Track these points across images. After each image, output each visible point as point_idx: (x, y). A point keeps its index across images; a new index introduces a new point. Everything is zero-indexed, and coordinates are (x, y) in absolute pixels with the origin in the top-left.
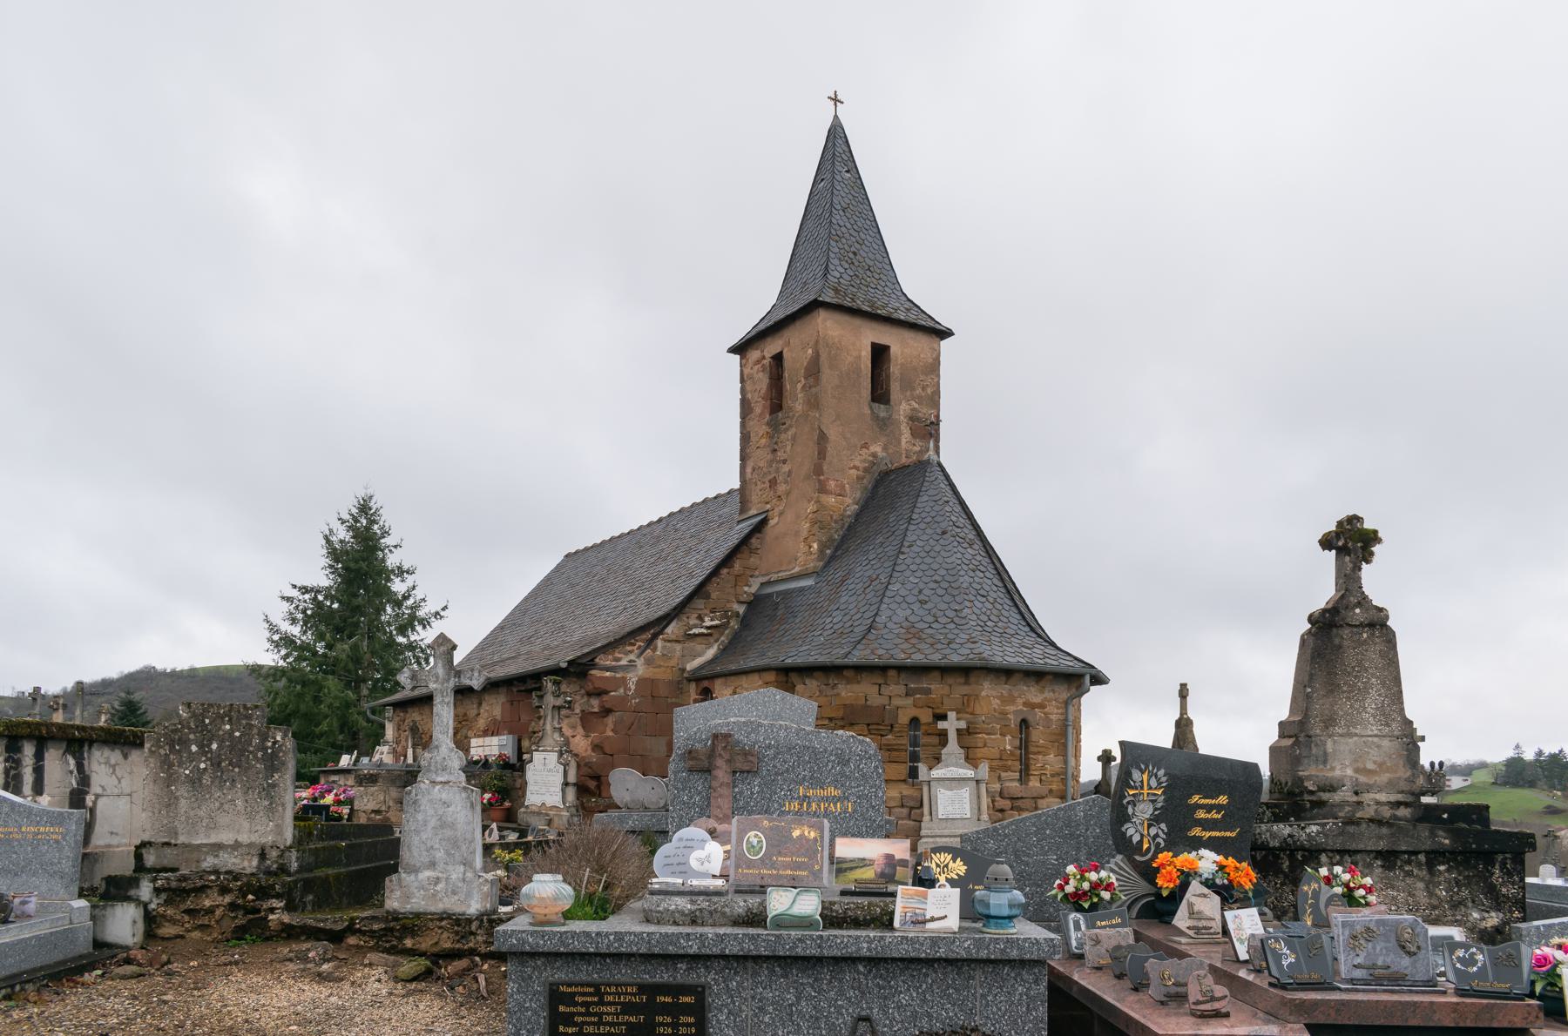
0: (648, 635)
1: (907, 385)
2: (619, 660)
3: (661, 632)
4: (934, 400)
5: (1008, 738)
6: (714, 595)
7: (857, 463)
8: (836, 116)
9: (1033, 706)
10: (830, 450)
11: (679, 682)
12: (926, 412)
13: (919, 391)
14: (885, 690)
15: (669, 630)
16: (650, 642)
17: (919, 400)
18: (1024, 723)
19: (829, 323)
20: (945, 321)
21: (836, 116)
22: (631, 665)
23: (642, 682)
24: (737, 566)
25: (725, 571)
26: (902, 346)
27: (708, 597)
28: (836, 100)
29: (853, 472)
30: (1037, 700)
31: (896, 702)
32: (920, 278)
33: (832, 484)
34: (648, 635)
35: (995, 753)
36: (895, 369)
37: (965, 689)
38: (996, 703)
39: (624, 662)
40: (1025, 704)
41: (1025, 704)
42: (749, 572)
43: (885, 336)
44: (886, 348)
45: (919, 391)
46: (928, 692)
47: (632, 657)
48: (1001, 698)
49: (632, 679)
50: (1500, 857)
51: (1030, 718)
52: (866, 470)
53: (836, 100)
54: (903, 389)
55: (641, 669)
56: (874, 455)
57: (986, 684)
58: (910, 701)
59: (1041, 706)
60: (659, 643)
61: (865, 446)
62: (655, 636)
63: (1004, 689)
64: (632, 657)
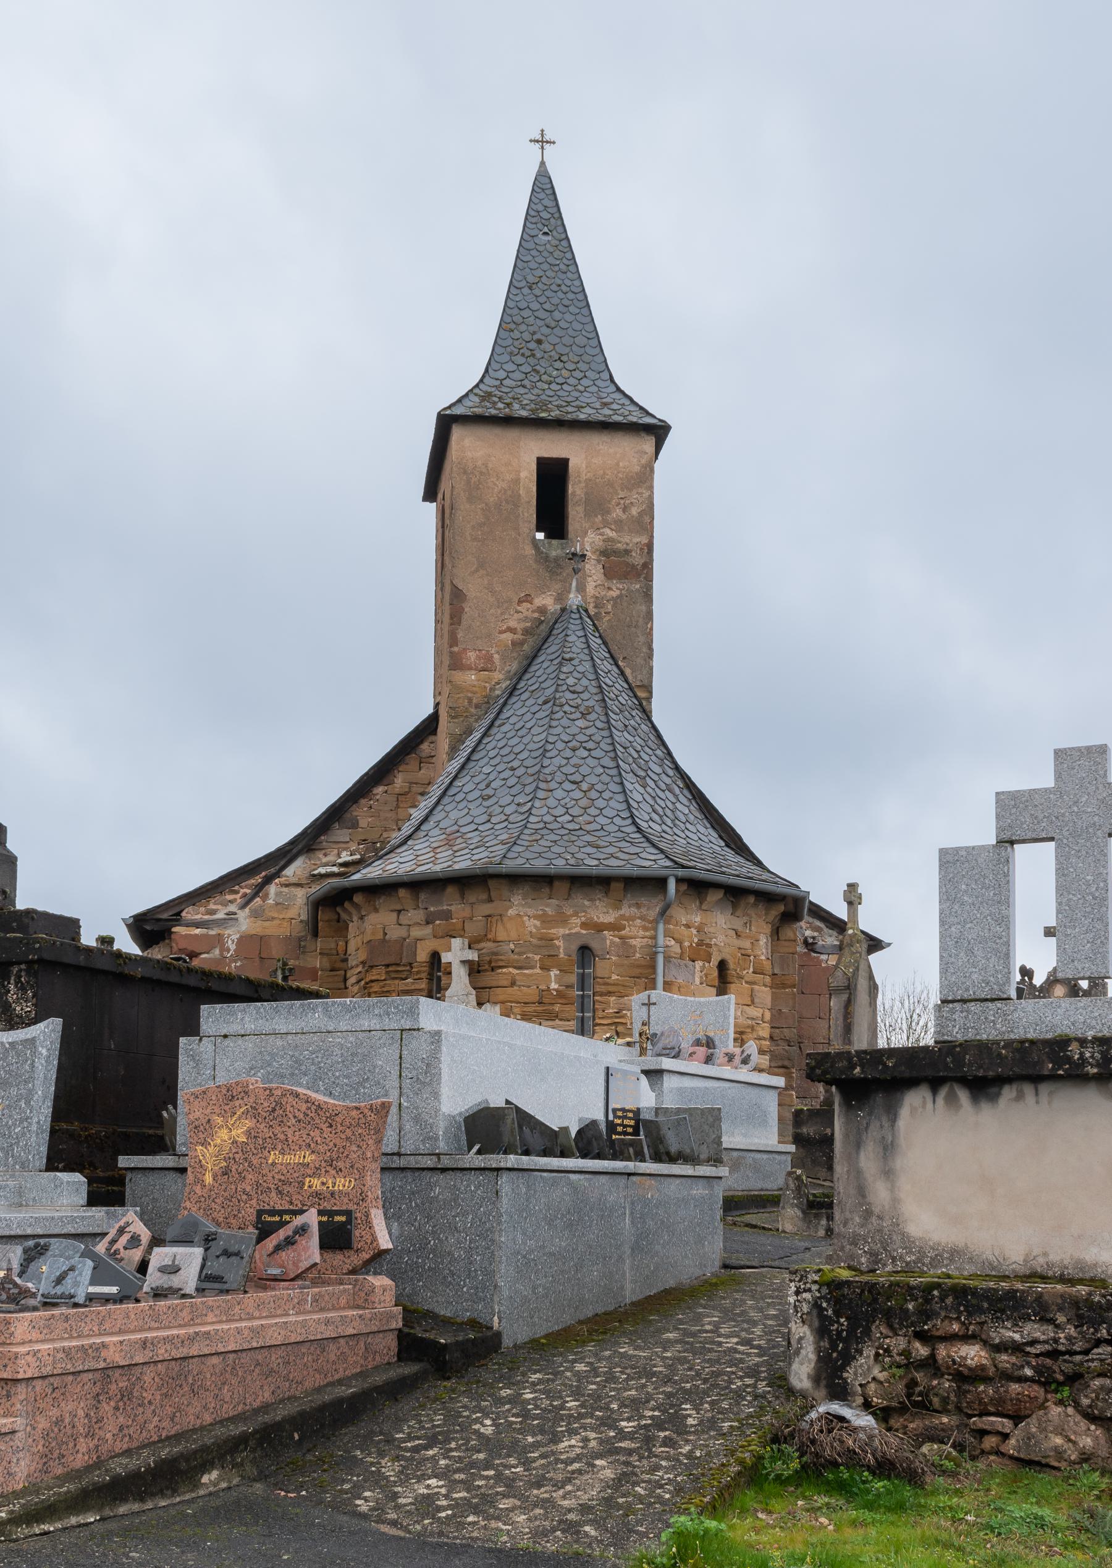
0: (258, 879)
1: (597, 506)
2: (213, 912)
3: (277, 875)
4: (645, 523)
5: (554, 973)
6: (363, 823)
7: (512, 624)
8: (543, 163)
9: (600, 928)
10: (469, 610)
11: (300, 939)
12: (630, 540)
13: (617, 513)
14: (405, 919)
15: (289, 871)
16: (259, 889)
17: (619, 525)
18: (585, 952)
19: (467, 442)
20: (660, 410)
21: (543, 163)
22: (231, 917)
23: (245, 940)
24: (400, 781)
25: (380, 790)
26: (584, 456)
27: (355, 825)
28: (542, 141)
29: (508, 637)
30: (609, 918)
31: (416, 932)
32: (639, 362)
33: (472, 656)
34: (258, 879)
35: (531, 993)
36: (575, 489)
37: (487, 909)
38: (532, 925)
39: (220, 915)
40: (584, 925)
41: (584, 925)
42: (416, 789)
43: (554, 446)
44: (563, 463)
45: (617, 513)
46: (447, 916)
47: (232, 908)
48: (544, 919)
49: (232, 937)
50: (15, 969)
51: (594, 945)
52: (526, 632)
53: (542, 141)
54: (588, 514)
55: (245, 923)
56: (542, 610)
57: (517, 899)
58: (428, 930)
59: (615, 927)
60: (272, 889)
61: (528, 599)
62: (268, 880)
63: (549, 907)
64: (232, 908)
